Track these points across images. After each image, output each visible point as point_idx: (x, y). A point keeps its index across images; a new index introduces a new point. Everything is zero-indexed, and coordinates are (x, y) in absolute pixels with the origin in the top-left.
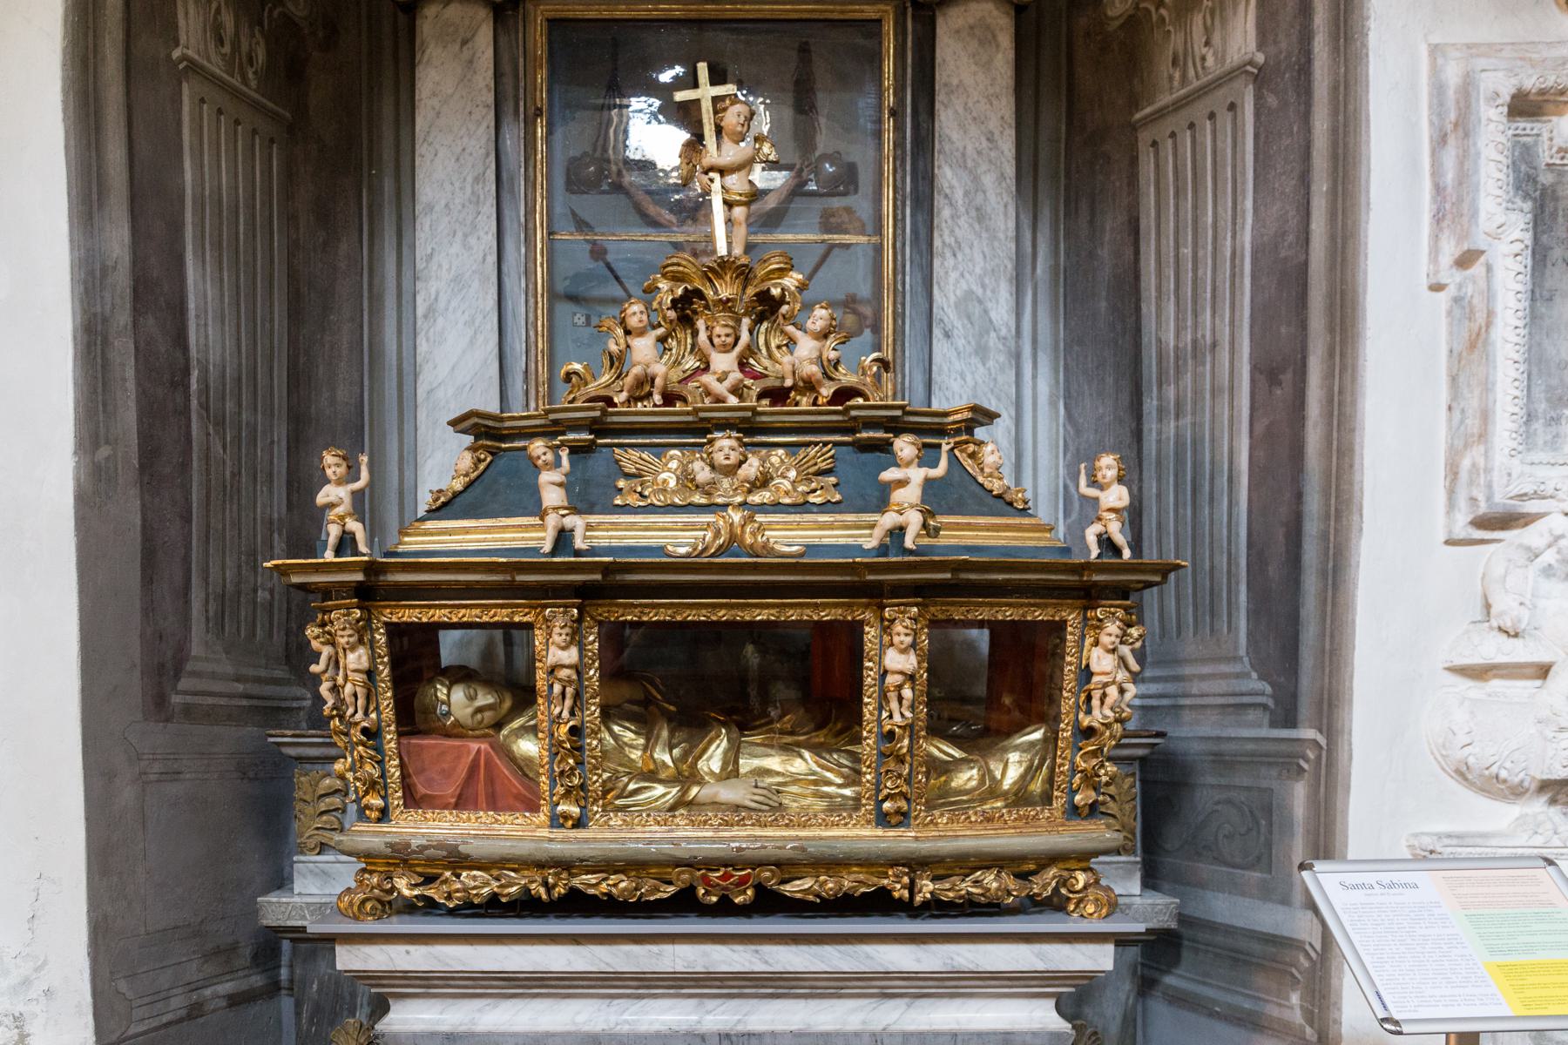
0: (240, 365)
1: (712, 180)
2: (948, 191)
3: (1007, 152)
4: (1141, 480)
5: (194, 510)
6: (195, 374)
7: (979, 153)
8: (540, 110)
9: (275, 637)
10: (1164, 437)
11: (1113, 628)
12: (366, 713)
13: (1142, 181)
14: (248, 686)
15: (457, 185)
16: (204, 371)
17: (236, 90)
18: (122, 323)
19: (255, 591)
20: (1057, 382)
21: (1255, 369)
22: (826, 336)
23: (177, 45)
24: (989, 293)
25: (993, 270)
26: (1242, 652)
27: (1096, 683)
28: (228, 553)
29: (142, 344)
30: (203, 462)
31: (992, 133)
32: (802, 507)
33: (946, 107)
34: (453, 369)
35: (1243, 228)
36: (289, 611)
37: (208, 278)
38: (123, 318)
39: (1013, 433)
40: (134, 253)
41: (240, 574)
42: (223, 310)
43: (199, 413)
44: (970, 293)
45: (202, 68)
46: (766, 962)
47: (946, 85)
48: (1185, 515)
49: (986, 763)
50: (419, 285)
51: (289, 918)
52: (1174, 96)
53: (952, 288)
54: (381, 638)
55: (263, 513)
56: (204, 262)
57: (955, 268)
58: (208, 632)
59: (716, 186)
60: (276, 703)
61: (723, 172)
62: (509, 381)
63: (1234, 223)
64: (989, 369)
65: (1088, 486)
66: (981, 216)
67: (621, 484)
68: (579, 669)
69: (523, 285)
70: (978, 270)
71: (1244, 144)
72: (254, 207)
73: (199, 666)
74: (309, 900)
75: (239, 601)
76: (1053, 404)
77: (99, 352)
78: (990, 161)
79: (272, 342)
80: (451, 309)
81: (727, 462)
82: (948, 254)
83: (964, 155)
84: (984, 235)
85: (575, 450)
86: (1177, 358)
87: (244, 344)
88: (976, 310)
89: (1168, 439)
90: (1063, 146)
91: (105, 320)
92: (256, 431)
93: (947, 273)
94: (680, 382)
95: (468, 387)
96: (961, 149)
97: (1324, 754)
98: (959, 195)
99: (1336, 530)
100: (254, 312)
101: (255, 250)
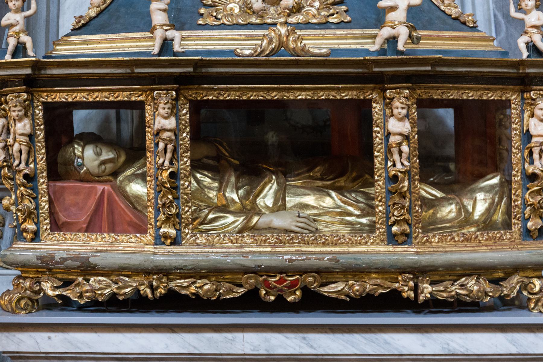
12: (27, 164)
32: (325, 25)
46: (311, 347)
54: (39, 113)
67: (202, 11)
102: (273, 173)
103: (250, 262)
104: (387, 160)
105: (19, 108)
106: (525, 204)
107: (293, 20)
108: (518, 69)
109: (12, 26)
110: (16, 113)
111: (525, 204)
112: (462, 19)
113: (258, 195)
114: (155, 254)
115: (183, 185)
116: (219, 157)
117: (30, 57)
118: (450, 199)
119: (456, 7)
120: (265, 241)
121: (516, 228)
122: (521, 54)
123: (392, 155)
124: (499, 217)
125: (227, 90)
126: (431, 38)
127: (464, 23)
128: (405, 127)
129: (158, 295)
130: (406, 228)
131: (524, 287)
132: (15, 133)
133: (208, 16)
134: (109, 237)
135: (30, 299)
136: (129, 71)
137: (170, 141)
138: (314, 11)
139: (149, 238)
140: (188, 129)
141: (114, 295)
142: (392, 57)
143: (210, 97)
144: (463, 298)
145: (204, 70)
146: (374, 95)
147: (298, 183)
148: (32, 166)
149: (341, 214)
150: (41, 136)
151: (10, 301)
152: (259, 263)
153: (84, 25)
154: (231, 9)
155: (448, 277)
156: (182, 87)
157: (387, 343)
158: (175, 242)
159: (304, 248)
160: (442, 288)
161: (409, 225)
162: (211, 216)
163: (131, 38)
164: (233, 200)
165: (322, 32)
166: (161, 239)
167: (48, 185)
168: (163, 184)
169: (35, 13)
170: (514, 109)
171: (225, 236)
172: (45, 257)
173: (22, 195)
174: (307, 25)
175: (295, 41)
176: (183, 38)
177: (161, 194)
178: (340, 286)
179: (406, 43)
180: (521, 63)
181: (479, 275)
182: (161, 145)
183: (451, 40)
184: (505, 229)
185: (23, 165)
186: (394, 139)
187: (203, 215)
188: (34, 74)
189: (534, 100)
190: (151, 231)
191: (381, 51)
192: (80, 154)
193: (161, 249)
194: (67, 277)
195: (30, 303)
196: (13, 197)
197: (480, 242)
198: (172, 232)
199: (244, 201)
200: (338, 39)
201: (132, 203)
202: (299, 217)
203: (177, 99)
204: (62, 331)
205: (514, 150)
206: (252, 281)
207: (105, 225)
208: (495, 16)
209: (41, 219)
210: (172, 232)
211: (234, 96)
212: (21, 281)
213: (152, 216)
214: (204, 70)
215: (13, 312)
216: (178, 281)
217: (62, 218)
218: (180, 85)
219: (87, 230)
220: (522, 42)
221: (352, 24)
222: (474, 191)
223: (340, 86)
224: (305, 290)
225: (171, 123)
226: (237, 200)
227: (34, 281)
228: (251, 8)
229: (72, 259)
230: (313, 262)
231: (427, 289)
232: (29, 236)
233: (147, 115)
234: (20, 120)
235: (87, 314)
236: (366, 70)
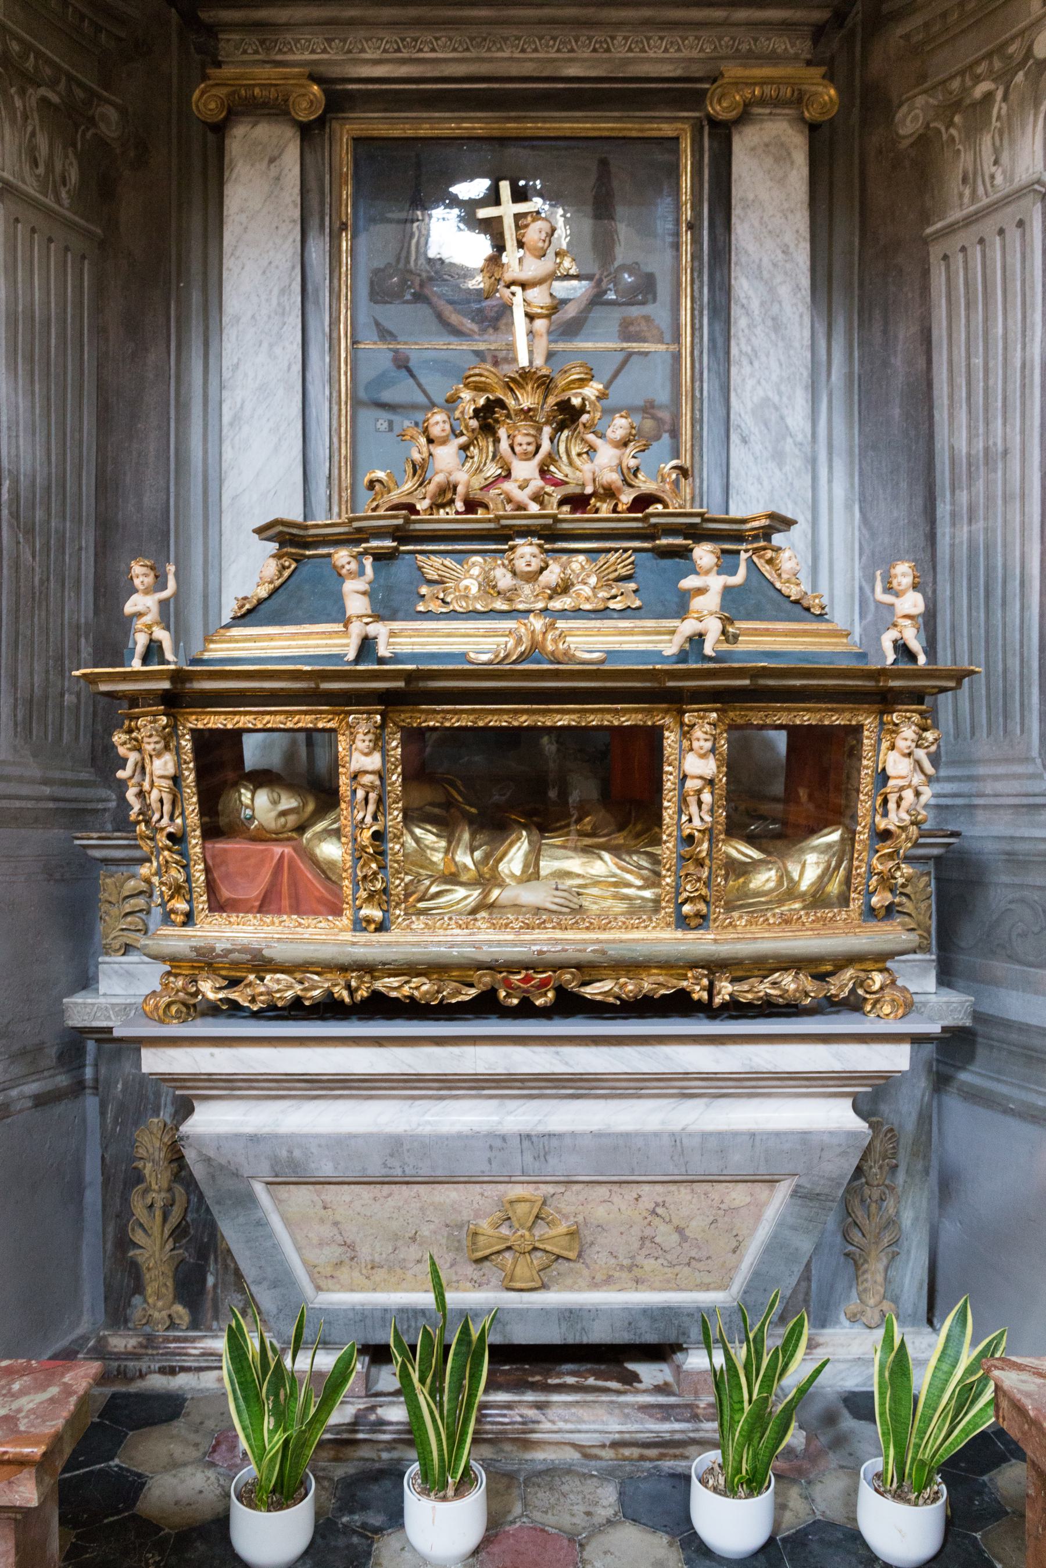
0: (49, 474)
1: (513, 294)
2: (744, 301)
3: (801, 264)
4: (935, 582)
7: (775, 265)
9: (82, 740)
10: (957, 541)
12: (172, 818)
15: (264, 297)
16: (15, 481)
19: (62, 695)
20: (852, 485)
24: (785, 399)
26: (1035, 753)
27: (893, 787)
32: (602, 613)
33: (742, 221)
41: (47, 679)
46: (567, 1064)
47: (741, 199)
48: (978, 617)
51: (94, 1018)
52: (965, 212)
54: (186, 744)
55: (70, 618)
57: (752, 375)
58: (16, 736)
60: (82, 805)
61: (524, 286)
62: (312, 486)
63: (1024, 335)
66: (777, 325)
67: (424, 590)
69: (327, 393)
70: (774, 378)
71: (1032, 258)
74: (114, 1001)
76: (849, 507)
78: (786, 273)
79: (81, 452)
81: (529, 569)
82: (745, 362)
83: (759, 267)
84: (781, 344)
86: (969, 465)
88: (774, 417)
90: (856, 258)
92: (64, 536)
93: (743, 380)
94: (481, 489)
98: (755, 305)
102: (525, 826)
103: (485, 954)
104: (680, 812)
105: (155, 739)
106: (871, 872)
107: (557, 604)
108: (878, 681)
109: (139, 615)
110: (152, 746)
111: (871, 872)
112: (805, 603)
113: (501, 859)
114: (354, 944)
115: (392, 849)
116: (449, 804)
117: (169, 663)
118: (770, 862)
119: (798, 585)
120: (506, 926)
121: (856, 903)
122: (885, 657)
123: (687, 806)
124: (834, 888)
125: (455, 712)
126: (756, 632)
127: (808, 609)
128: (709, 767)
130: (702, 907)
131: (860, 983)
132: (151, 775)
133: (431, 599)
134: (290, 920)
135: (185, 1004)
136: (313, 685)
137: (373, 787)
138: (587, 591)
139: (345, 921)
140: (399, 770)
141: (297, 1001)
142: (694, 666)
143: (431, 724)
144: (774, 1000)
145: (421, 684)
146: (668, 720)
147: (558, 841)
148: (179, 821)
149: (616, 885)
150: (190, 777)
151: (156, 1007)
152: (496, 957)
153: (249, 611)
154: (467, 588)
155: (756, 973)
156: (390, 708)
157: (667, 1057)
158: (382, 927)
159: (559, 935)
160: (746, 987)
161: (707, 903)
162: (434, 889)
164: (465, 866)
165: (597, 623)
166: (360, 925)
167: (203, 848)
168: (363, 848)
169: (176, 595)
170: (868, 738)
171: (450, 919)
172: (201, 948)
173: (167, 862)
174: (577, 613)
175: (555, 641)
176: (392, 634)
177: (362, 862)
178: (607, 985)
179: (718, 641)
180: (883, 673)
181: (799, 969)
182: (360, 794)
183: (786, 636)
184: (841, 906)
185: (165, 821)
186: (691, 784)
187: (422, 888)
188: (175, 688)
189: (896, 725)
190: (348, 912)
191: (682, 656)
192: (249, 802)
193: (362, 937)
194: (233, 973)
195: (184, 1010)
196: (155, 864)
197: (803, 924)
198: (377, 914)
199: (481, 867)
200: (621, 635)
201: (324, 872)
202: (557, 889)
203: (383, 726)
204: (230, 1046)
205: (862, 797)
206: (487, 979)
207: (285, 903)
208: (861, 589)
209: (195, 895)
210: (377, 914)
211: (466, 721)
212: (172, 979)
213: (349, 892)
214: (421, 684)
215: (161, 1021)
216: (386, 980)
217: (226, 893)
218: (387, 705)
219: (259, 912)
220: (887, 641)
221: (642, 611)
222: (803, 851)
223: (619, 706)
224: (560, 990)
225: (374, 761)
226: (472, 866)
227: (188, 979)
228: (494, 587)
229: (239, 951)
230: (572, 954)
231: (725, 989)
232: (180, 919)
233: (340, 749)
234: (159, 755)
235: (262, 1022)
236: (656, 685)
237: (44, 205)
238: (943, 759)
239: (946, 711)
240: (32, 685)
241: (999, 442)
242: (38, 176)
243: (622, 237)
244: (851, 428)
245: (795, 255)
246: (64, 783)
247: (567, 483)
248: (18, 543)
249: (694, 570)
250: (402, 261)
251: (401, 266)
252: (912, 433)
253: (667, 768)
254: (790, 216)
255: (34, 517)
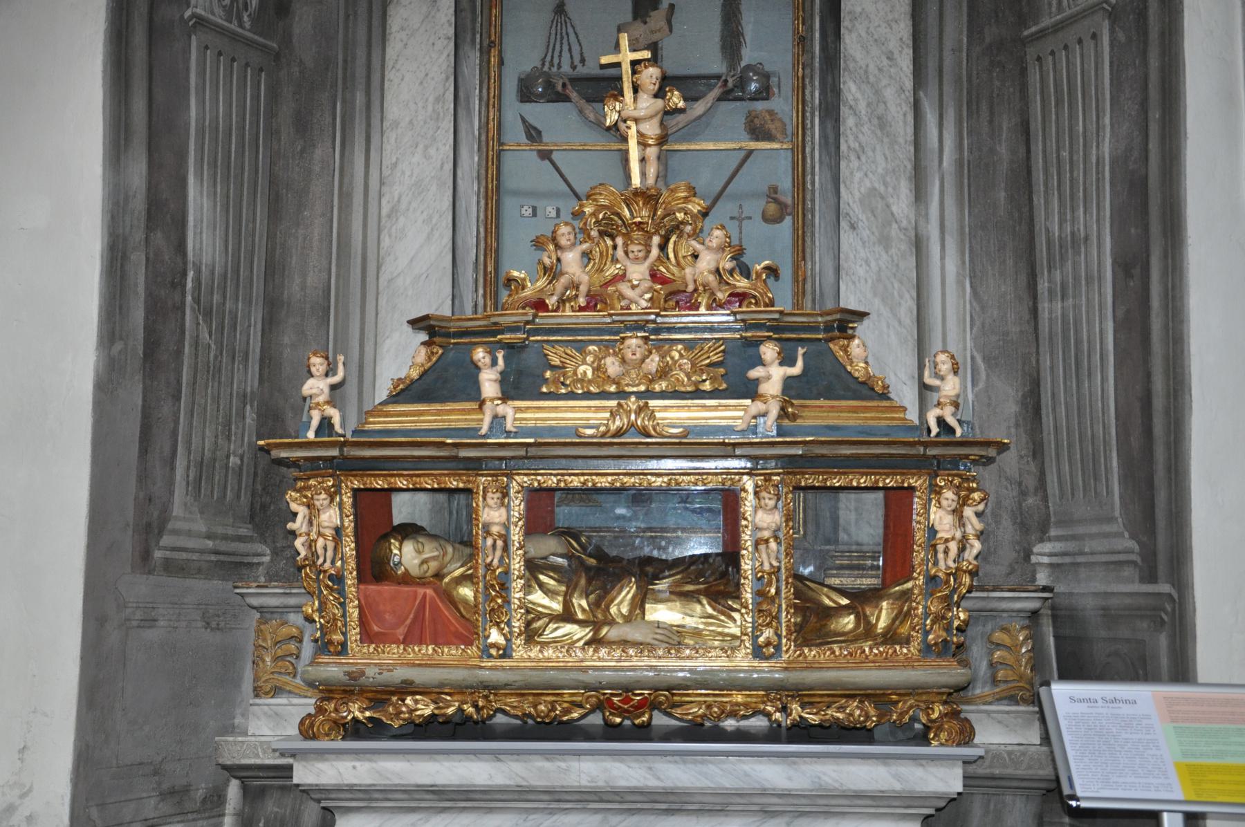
0: (227, 262)
1: (629, 128)
2: (852, 103)
3: (905, 68)
4: (1038, 353)
5: (184, 389)
6: (191, 274)
7: (880, 70)
8: (493, 42)
9: (242, 498)
10: (1054, 315)
11: (949, 495)
12: (333, 562)
13: (1031, 90)
14: (218, 542)
15: (420, 104)
16: (198, 272)
17: (234, 33)
18: (137, 240)
19: (228, 457)
20: (964, 263)
21: (1114, 262)
22: (723, 250)
23: (188, 6)
24: (890, 189)
25: (894, 170)
26: (1117, 513)
27: (941, 538)
28: (208, 424)
29: (151, 256)
30: (193, 349)
31: (891, 52)
32: (698, 394)
33: (850, 31)
34: (411, 261)
35: (1104, 140)
36: (255, 474)
37: (205, 193)
38: (139, 236)
39: (915, 312)
40: (150, 182)
41: (216, 443)
42: (215, 218)
43: (192, 307)
44: (873, 189)
45: (208, 21)
46: (658, 778)
47: (850, 13)
48: (1071, 386)
49: (863, 609)
50: (385, 189)
51: (243, 757)
52: (1053, 20)
53: (857, 186)
54: (347, 500)
55: (238, 388)
56: (202, 180)
57: (859, 169)
58: (187, 494)
59: (634, 128)
60: (238, 559)
61: (636, 120)
62: (460, 270)
63: (1098, 135)
64: (892, 257)
65: (930, 377)
66: (882, 123)
67: (548, 374)
68: (507, 527)
69: (476, 188)
70: (880, 170)
71: (1103, 69)
72: (244, 128)
73: (179, 525)
74: (263, 739)
75: (214, 467)
76: (960, 284)
77: (119, 265)
78: (891, 77)
79: (253, 241)
80: (411, 210)
81: (634, 357)
82: (853, 157)
83: (866, 72)
84: (886, 140)
85: (510, 347)
86: (1061, 247)
87: (230, 243)
88: (880, 205)
89: (1057, 317)
90: (964, 54)
91: (125, 239)
92: (236, 317)
93: (852, 173)
94: (601, 286)
95: (425, 275)
96: (864, 66)
97: (1177, 606)
98: (862, 106)
99: (1175, 407)
100: (241, 216)
101: (243, 163)
129: (294, 506)
153: (402, 390)
163: (459, 410)
170: (919, 497)
185: (327, 565)
208: (973, 358)
237: (227, 30)
238: (1053, 520)
239: (1052, 473)
240: (203, 449)
241: (1082, 228)
242: (224, 7)
243: (748, 38)
244: (961, 211)
245: (899, 60)
246: (225, 538)
247: (674, 281)
248: (198, 324)
249: (760, 362)
250: (547, 64)
251: (546, 69)
252: (1016, 215)
253: (744, 523)
254: (894, 26)
255: (212, 300)
